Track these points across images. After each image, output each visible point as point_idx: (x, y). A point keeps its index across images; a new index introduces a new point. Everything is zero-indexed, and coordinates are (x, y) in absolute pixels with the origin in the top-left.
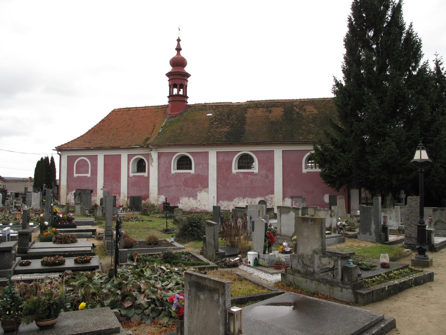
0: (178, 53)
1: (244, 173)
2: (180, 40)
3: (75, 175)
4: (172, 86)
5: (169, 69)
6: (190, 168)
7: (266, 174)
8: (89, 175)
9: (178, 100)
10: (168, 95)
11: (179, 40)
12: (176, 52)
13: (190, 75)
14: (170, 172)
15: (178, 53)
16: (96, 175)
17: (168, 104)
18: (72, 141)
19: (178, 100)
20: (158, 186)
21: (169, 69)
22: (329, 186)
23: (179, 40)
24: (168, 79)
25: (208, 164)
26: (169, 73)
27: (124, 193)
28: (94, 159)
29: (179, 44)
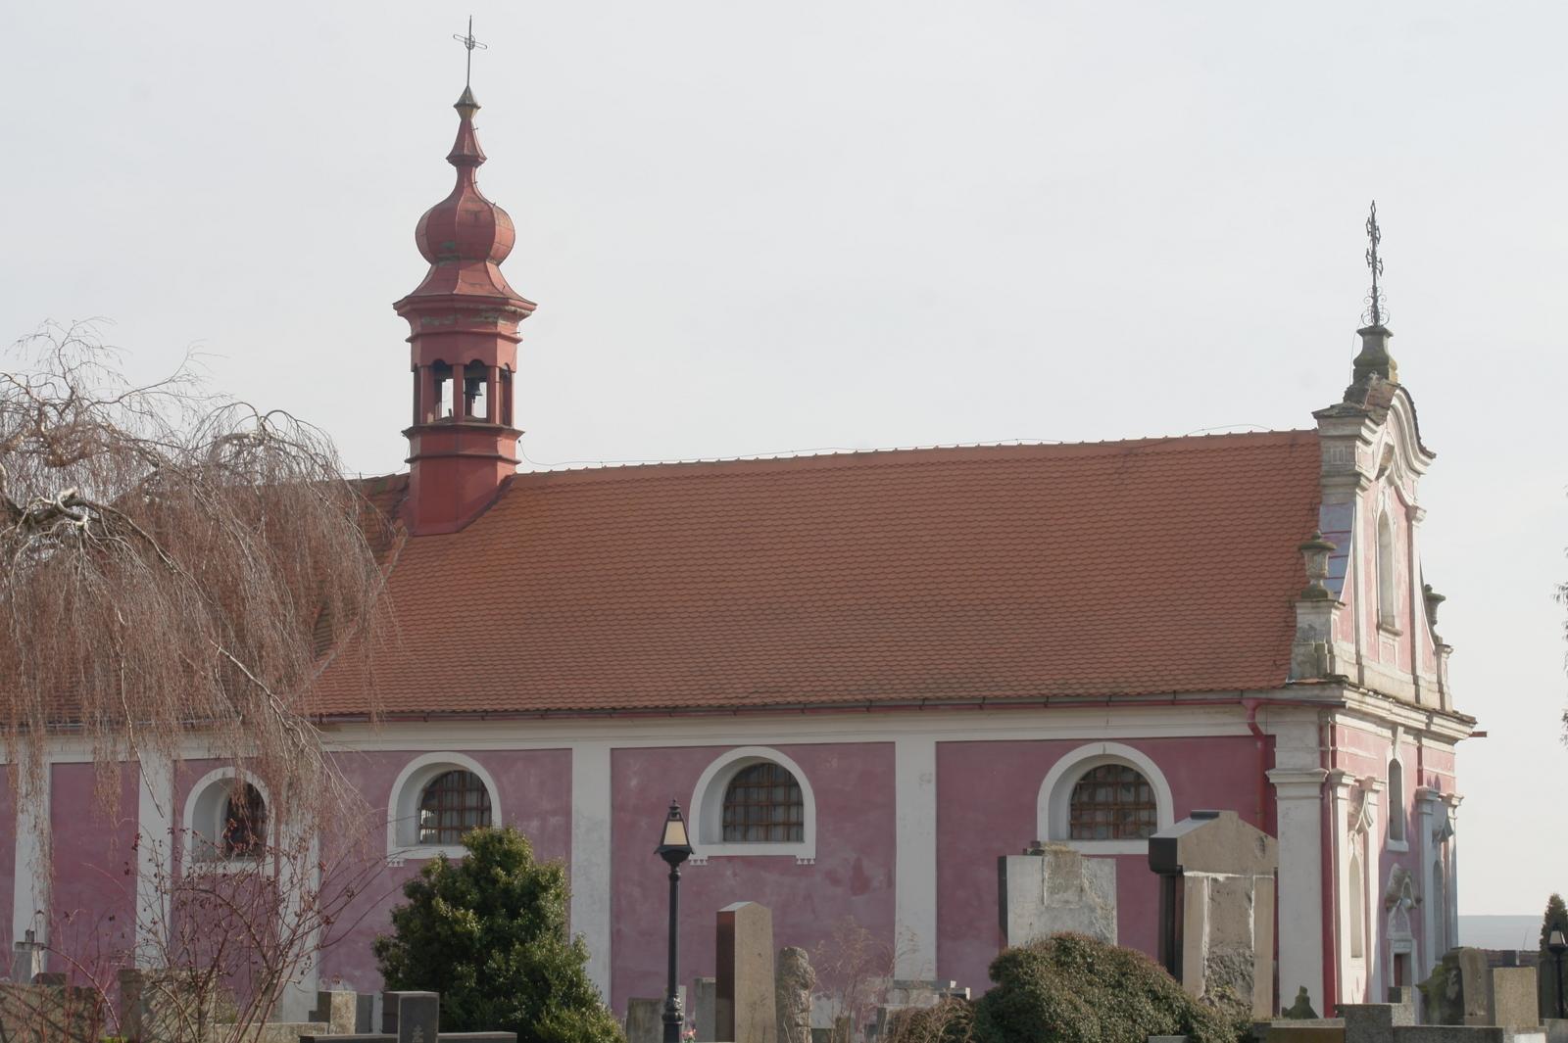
0: (465, 181)
1: (747, 861)
2: (475, 106)
4: (429, 374)
5: (414, 271)
7: (858, 868)
9: (458, 444)
10: (409, 423)
11: (466, 106)
12: (451, 174)
13: (531, 307)
15: (465, 181)
17: (407, 469)
19: (458, 444)
21: (414, 271)
22: (1042, 938)
23: (466, 106)
24: (404, 328)
25: (567, 812)
28: (868, 787)
29: (466, 130)
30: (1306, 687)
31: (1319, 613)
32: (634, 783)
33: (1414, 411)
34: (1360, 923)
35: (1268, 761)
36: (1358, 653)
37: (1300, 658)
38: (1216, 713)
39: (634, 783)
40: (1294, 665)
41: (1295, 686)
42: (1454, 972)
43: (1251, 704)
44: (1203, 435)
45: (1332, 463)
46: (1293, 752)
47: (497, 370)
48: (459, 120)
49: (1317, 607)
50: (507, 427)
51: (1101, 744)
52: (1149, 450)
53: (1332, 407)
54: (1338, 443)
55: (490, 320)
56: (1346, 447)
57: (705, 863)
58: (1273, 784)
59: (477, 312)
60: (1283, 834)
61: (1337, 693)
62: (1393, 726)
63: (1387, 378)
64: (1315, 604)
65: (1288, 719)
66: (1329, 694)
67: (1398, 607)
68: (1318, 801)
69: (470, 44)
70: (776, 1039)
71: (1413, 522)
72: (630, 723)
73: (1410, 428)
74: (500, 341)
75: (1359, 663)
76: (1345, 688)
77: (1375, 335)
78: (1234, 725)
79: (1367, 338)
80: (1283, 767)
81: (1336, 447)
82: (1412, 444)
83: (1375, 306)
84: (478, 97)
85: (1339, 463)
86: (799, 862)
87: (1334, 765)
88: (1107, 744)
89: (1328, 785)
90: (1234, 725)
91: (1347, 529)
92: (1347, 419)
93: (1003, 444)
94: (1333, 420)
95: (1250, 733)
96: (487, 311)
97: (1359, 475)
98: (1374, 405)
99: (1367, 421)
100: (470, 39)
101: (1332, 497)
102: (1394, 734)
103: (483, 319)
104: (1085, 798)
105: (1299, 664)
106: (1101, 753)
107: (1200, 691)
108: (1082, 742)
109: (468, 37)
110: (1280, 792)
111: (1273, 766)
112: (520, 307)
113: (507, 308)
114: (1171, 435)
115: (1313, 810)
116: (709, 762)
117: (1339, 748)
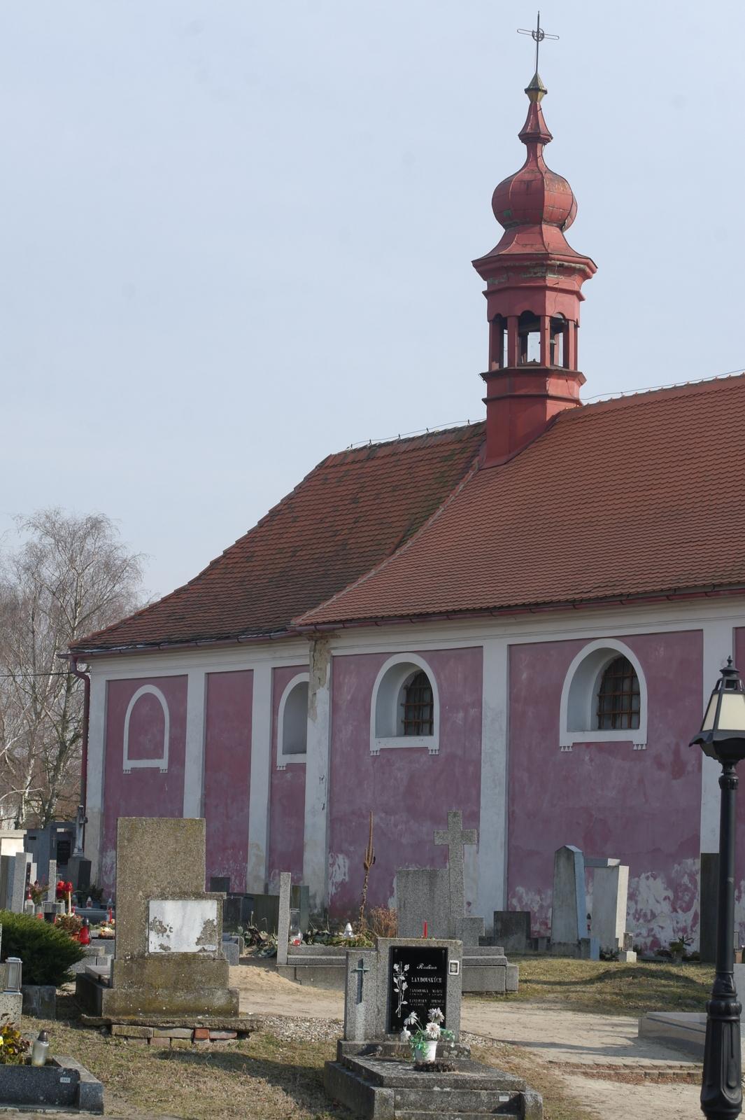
3: (128, 765)
6: (633, 724)
8: (162, 764)
11: (534, 91)
14: (368, 744)
15: (533, 155)
16: (182, 763)
18: (190, 583)
20: (330, 813)
21: (488, 234)
23: (534, 91)
26: (478, 260)
27: (257, 846)
29: (534, 110)
32: (524, 676)
34: (441, 713)
39: (524, 676)
47: (547, 320)
48: (530, 102)
50: (567, 370)
55: (539, 275)
57: (571, 750)
59: (525, 269)
69: (539, 36)
70: (532, 914)
72: (513, 620)
74: (548, 293)
84: (545, 83)
86: (635, 748)
96: (534, 267)
100: (538, 32)
103: (532, 275)
109: (536, 31)
112: (573, 263)
113: (549, 262)
116: (580, 648)
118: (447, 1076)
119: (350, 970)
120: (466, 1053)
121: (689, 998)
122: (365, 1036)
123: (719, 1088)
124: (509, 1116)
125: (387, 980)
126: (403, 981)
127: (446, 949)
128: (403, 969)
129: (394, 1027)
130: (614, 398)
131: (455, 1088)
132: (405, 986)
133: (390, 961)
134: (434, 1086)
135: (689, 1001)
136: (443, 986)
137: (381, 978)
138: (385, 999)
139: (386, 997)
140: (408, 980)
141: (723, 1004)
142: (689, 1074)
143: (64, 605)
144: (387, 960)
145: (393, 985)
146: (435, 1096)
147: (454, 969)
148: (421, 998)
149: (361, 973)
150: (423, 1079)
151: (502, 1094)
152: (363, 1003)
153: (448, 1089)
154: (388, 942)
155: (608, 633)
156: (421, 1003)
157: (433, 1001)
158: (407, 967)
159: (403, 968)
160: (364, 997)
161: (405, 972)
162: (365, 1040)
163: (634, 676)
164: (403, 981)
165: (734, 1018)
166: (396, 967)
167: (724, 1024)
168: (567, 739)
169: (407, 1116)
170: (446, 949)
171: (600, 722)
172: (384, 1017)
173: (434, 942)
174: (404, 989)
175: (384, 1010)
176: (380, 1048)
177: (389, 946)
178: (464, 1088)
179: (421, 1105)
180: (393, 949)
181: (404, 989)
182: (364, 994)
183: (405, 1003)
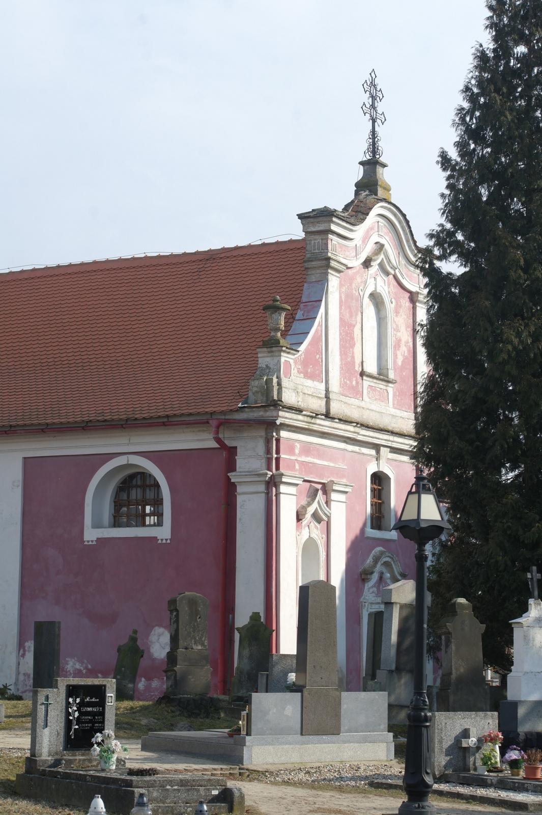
30: (254, 409)
31: (272, 356)
33: (407, 222)
35: (231, 466)
36: (327, 390)
37: (255, 389)
38: (199, 431)
40: (250, 394)
41: (246, 410)
42: (175, 613)
43: (214, 423)
44: (260, 243)
45: (313, 252)
46: (248, 460)
49: (272, 352)
51: (125, 457)
52: (228, 254)
53: (313, 210)
54: (317, 237)
56: (322, 239)
58: (234, 483)
60: (240, 519)
61: (274, 414)
62: (377, 447)
63: (376, 195)
64: (269, 350)
65: (245, 435)
66: (269, 414)
67: (395, 362)
68: (263, 495)
71: (417, 304)
73: (405, 234)
75: (327, 397)
76: (280, 410)
77: (372, 164)
78: (203, 440)
79: (366, 167)
80: (241, 470)
81: (315, 240)
82: (409, 247)
83: (374, 144)
85: (317, 251)
87: (278, 468)
88: (131, 456)
89: (273, 483)
90: (203, 440)
91: (320, 299)
92: (321, 219)
93: (136, 256)
94: (312, 220)
95: (217, 446)
97: (329, 259)
98: (356, 212)
99: (334, 219)
101: (314, 276)
102: (378, 452)
104: (125, 496)
105: (254, 394)
106: (126, 463)
107: (182, 415)
108: (113, 455)
110: (240, 489)
111: (234, 470)
114: (240, 245)
115: (260, 501)
117: (282, 456)
118: (157, 778)
119: (39, 703)
120: (122, 763)
121: (124, 723)
122: (49, 753)
123: (421, 773)
124: (223, 804)
125: (64, 711)
126: (76, 711)
127: (105, 686)
128: (75, 701)
129: (69, 746)
130: (266, 242)
131: (181, 786)
132: (77, 714)
133: (66, 696)
134: (166, 785)
135: (125, 726)
136: (103, 714)
137: (60, 709)
138: (63, 725)
139: (63, 723)
140: (79, 710)
141: (423, 714)
142: (230, 773)
143: (261, 308)
144: (65, 695)
145: (68, 714)
146: (170, 793)
147: (110, 701)
148: (88, 723)
149: (47, 706)
150: (159, 781)
151: (214, 789)
152: (48, 728)
153: (176, 787)
154: (65, 682)
155: (131, 451)
156: (88, 726)
157: (96, 725)
158: (78, 700)
159: (76, 701)
160: (49, 724)
161: (77, 704)
162: (49, 756)
163: (157, 486)
164: (76, 711)
165: (428, 724)
166: (71, 700)
167: (423, 729)
168: (91, 535)
169: (156, 808)
170: (105, 686)
171: (115, 521)
172: (62, 738)
173: (97, 682)
174: (76, 717)
175: (62, 733)
176: (64, 762)
177: (65, 684)
178: (186, 786)
179: (161, 800)
180: (68, 686)
181: (76, 717)
182: (48, 721)
183: (77, 727)
